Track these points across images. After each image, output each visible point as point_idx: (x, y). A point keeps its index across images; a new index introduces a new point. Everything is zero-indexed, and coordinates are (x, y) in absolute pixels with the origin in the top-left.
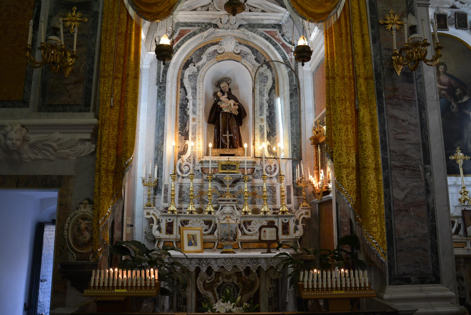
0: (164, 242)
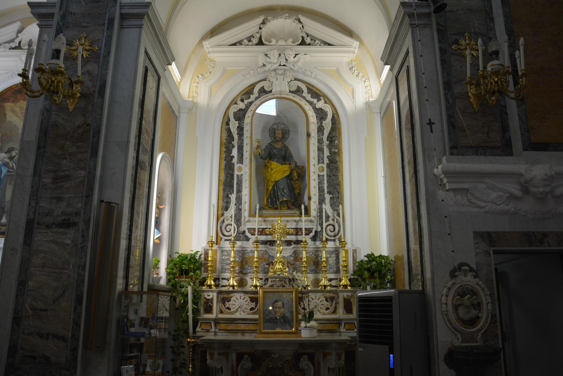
0: (345, 323)
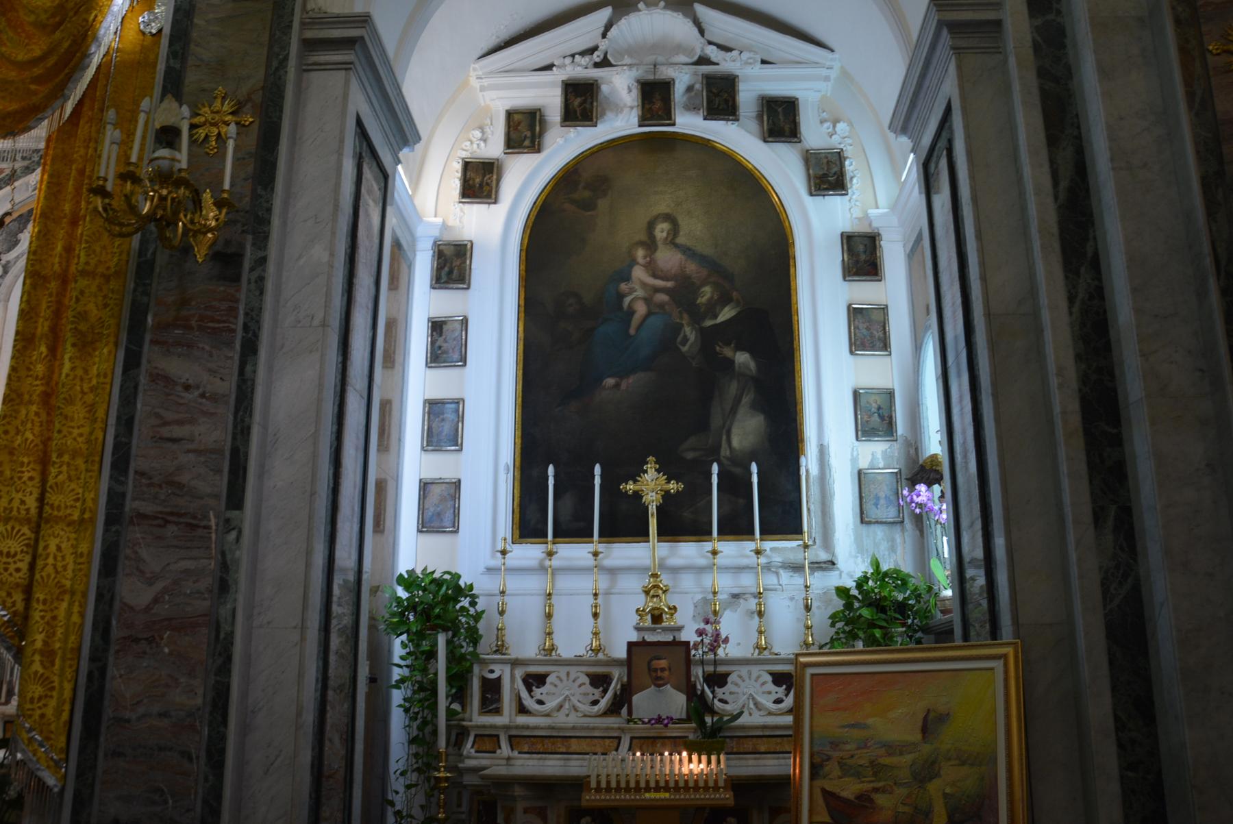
0: (476, 736)
